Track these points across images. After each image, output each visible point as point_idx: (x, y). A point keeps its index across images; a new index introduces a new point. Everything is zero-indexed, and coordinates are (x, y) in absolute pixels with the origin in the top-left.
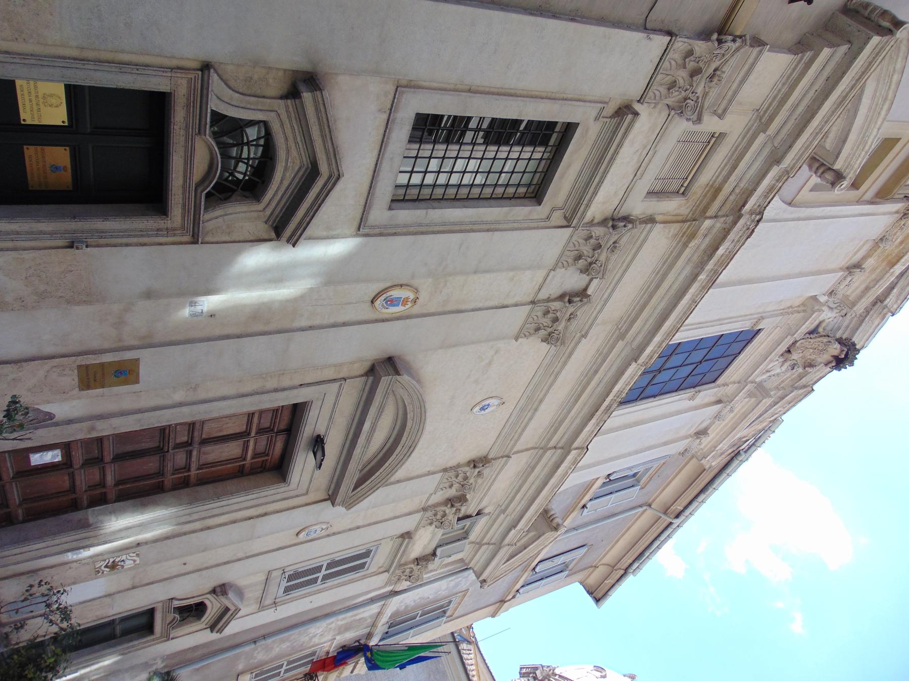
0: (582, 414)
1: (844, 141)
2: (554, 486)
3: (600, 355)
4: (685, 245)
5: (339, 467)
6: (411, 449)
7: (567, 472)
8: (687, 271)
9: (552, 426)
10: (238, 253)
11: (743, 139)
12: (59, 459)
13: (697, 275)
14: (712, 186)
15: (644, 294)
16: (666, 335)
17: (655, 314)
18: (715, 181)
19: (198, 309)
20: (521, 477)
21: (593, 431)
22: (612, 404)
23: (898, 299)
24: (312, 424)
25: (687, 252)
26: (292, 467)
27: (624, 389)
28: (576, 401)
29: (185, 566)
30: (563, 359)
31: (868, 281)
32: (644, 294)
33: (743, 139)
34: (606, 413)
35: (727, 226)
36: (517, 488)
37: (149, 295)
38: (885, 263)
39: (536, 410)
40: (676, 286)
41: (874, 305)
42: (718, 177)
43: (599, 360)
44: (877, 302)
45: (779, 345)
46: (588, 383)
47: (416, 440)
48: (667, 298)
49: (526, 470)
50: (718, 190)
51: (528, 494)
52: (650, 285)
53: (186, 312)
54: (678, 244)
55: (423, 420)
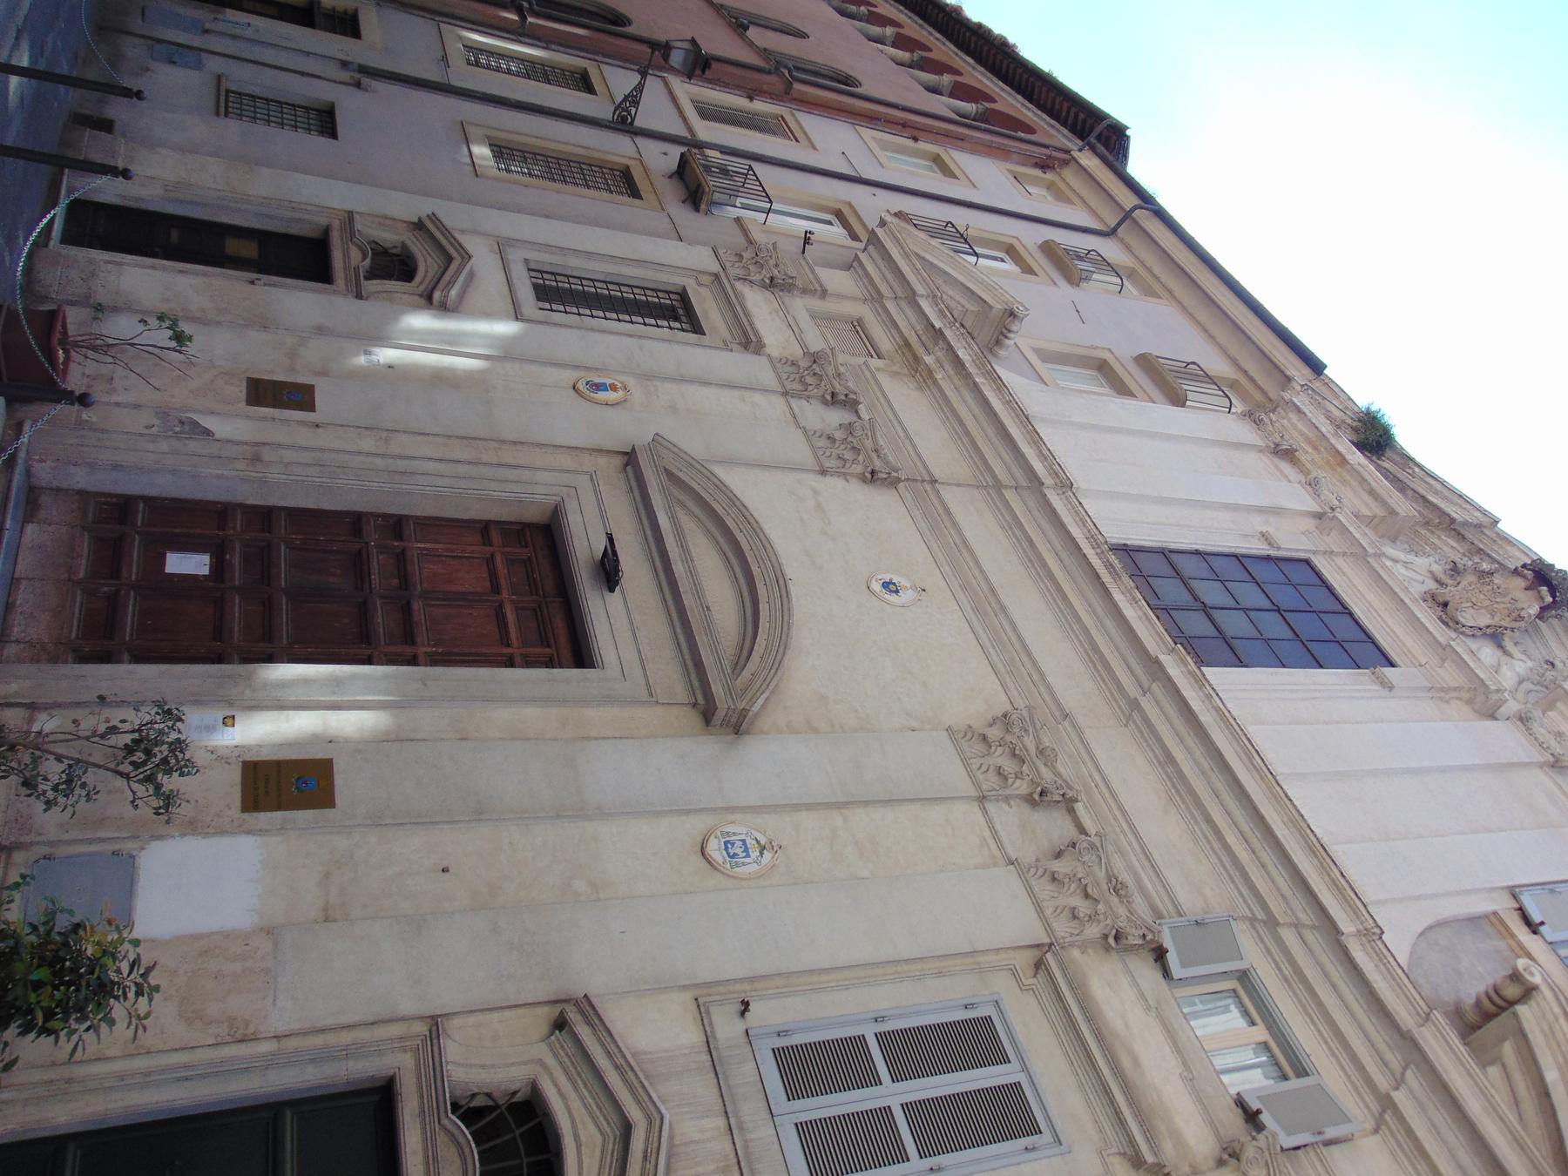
0: (1099, 610)
1: (973, 293)
2: (1247, 762)
3: (1010, 528)
4: (935, 382)
5: (679, 630)
6: (781, 582)
7: (1217, 709)
8: (968, 396)
9: (1095, 666)
10: (404, 313)
11: (879, 315)
12: (205, 571)
13: (975, 384)
14: (900, 347)
15: (962, 442)
16: (1016, 420)
17: (995, 439)
18: (897, 344)
19: (374, 358)
20: (1184, 802)
21: (1145, 614)
22: (1108, 561)
23: (1456, 504)
24: (584, 544)
25: (945, 385)
26: (591, 627)
27: (1089, 531)
28: (1065, 597)
29: (446, 875)
30: (948, 524)
31: (1360, 490)
32: (962, 442)
33: (879, 315)
34: (1120, 577)
35: (945, 347)
36: (1210, 834)
37: (320, 330)
38: (1339, 469)
39: (1003, 608)
40: (977, 410)
41: (1464, 538)
42: (895, 340)
43: (1018, 533)
44: (1455, 530)
45: (1380, 576)
46: (1044, 565)
47: (776, 565)
48: (985, 425)
49: (1168, 777)
50: (907, 344)
51: (1246, 828)
52: (954, 429)
53: (362, 360)
54: (930, 389)
55: (755, 525)
